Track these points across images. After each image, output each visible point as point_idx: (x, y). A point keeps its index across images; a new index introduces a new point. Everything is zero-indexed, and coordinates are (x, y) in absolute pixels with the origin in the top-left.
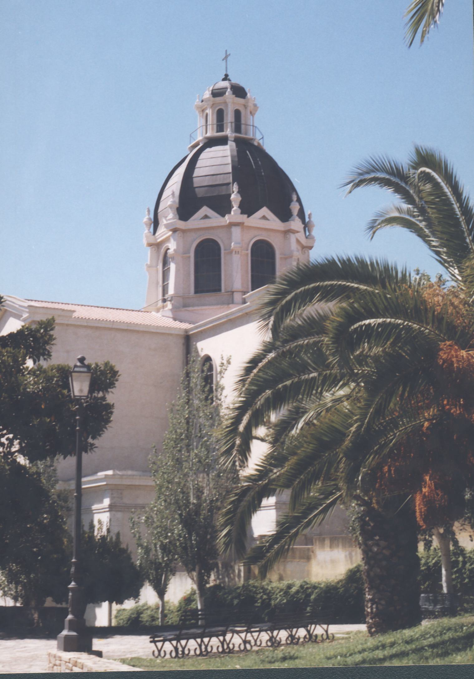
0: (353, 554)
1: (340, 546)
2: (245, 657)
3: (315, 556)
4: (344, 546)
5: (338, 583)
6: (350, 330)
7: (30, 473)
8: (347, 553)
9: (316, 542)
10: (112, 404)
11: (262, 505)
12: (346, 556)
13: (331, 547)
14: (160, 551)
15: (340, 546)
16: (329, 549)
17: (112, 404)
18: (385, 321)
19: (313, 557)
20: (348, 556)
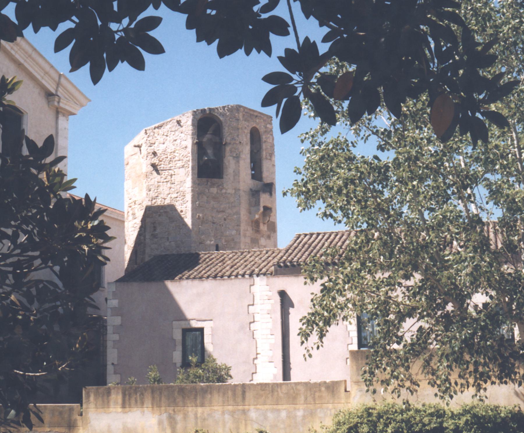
0: (179, 417)
1: (148, 402)
2: (336, 420)
3: (86, 423)
4: (156, 404)
5: (337, 388)
6: (465, 96)
7: (261, 193)
8: (165, 416)
9: (88, 396)
10: (379, 150)
11: (91, 296)
12: (160, 423)
13: (123, 406)
14: (491, 242)
15: (148, 402)
16: (120, 410)
17: (379, 150)
18: (289, 26)
19: (79, 423)
20: (166, 423)
